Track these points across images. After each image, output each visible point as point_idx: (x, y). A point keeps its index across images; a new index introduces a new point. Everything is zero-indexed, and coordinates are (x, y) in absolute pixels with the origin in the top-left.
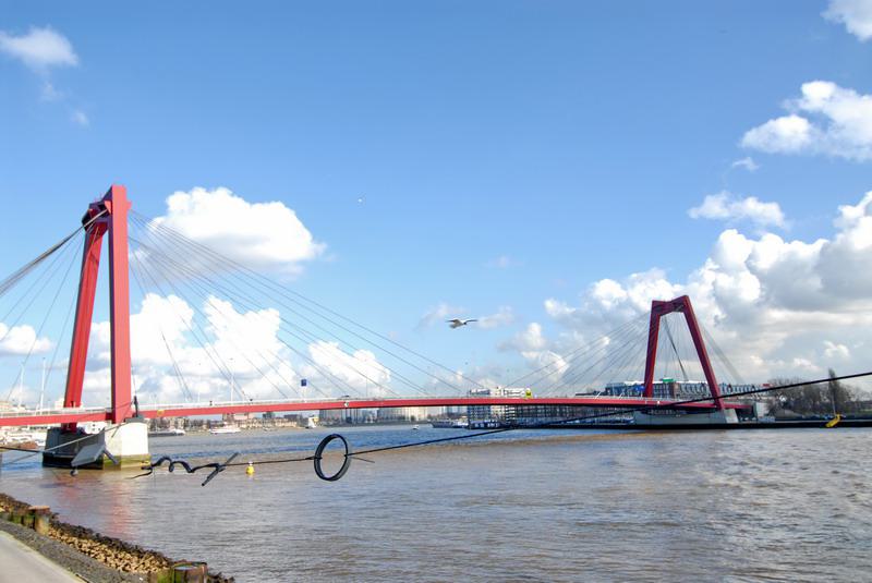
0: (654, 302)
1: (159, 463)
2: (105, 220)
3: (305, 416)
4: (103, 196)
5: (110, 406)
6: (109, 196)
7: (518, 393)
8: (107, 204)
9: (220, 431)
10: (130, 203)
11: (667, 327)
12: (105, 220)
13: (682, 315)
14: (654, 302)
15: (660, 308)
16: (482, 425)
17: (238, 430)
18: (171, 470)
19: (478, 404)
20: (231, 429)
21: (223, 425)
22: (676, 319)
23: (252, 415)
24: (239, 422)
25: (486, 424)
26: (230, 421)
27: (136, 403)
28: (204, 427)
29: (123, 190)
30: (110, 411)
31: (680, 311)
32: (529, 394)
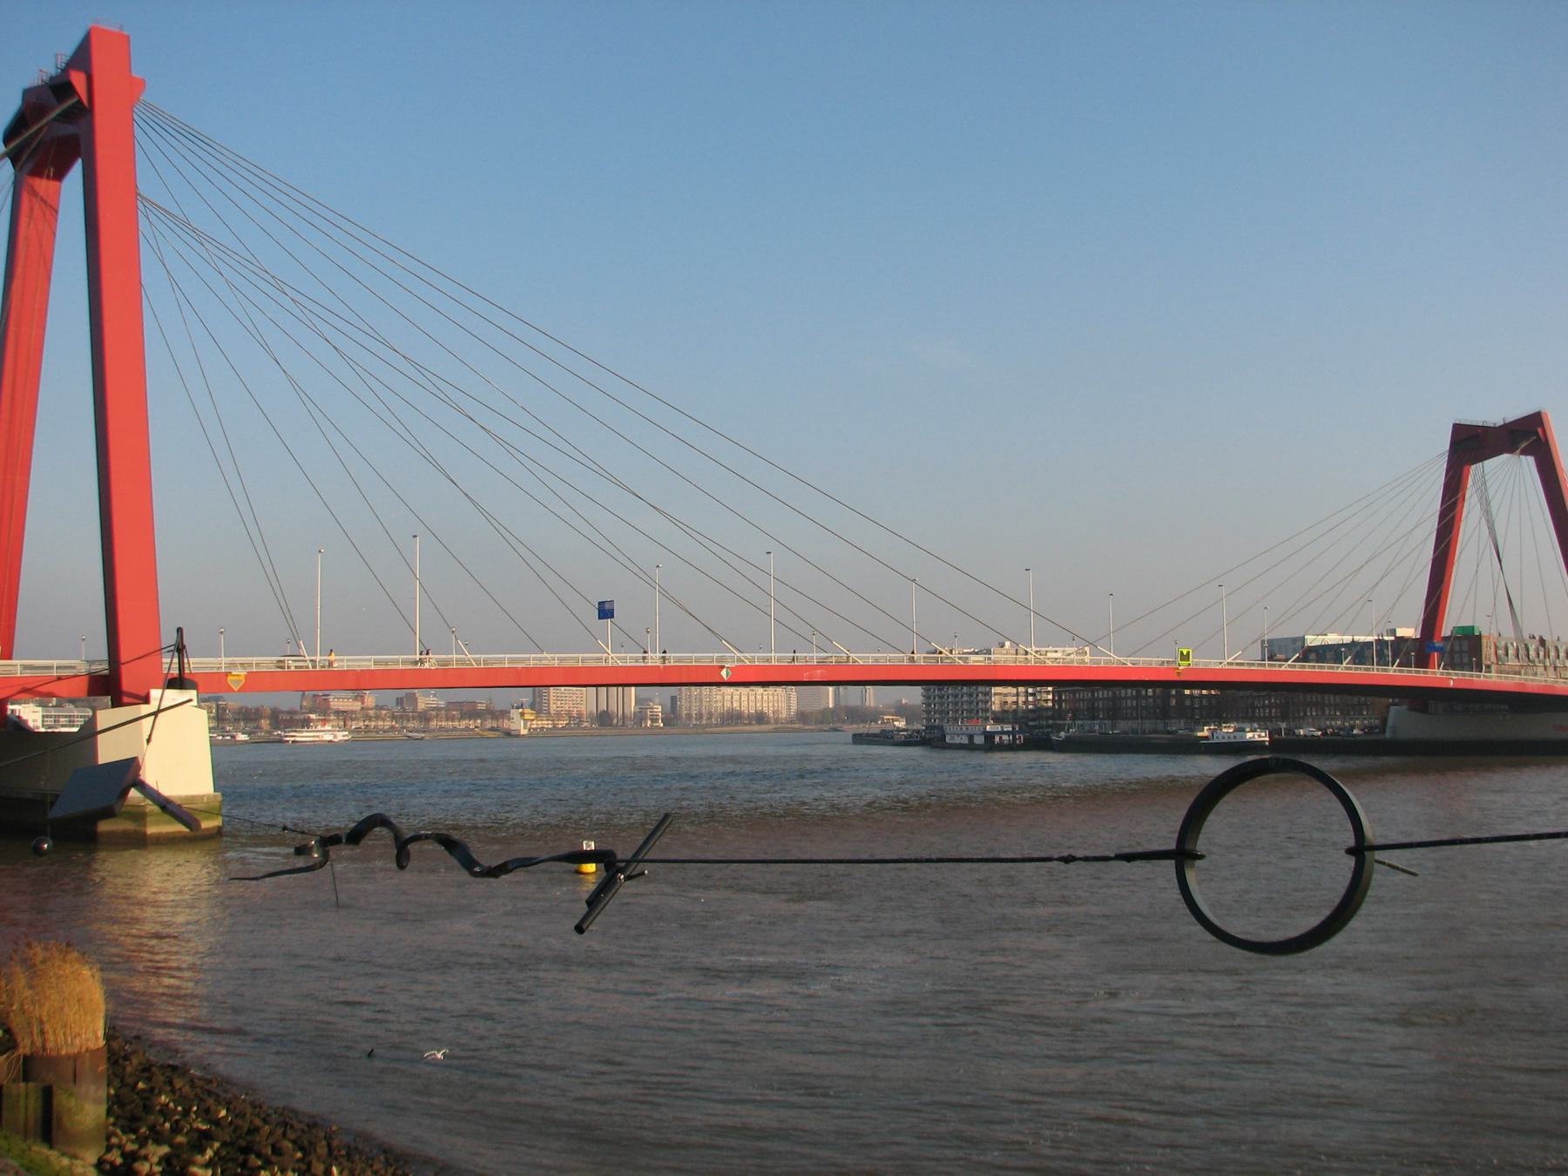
0: (1457, 428)
1: (355, 836)
2: (69, 129)
3: (498, 706)
4: (65, 59)
5: (103, 654)
6: (82, 58)
7: (1061, 656)
8: (78, 80)
9: (304, 736)
10: (141, 84)
11: (1486, 504)
12: (69, 129)
13: (1529, 461)
14: (1457, 428)
15: (1471, 444)
16: (979, 740)
17: (341, 736)
18: (402, 859)
19: (953, 691)
20: (327, 733)
21: (306, 723)
22: (1508, 481)
23: (370, 699)
24: (345, 716)
25: (989, 737)
26: (324, 711)
27: (180, 649)
28: (265, 723)
29: (123, 42)
30: (102, 667)
31: (1525, 452)
32: (1185, 657)
